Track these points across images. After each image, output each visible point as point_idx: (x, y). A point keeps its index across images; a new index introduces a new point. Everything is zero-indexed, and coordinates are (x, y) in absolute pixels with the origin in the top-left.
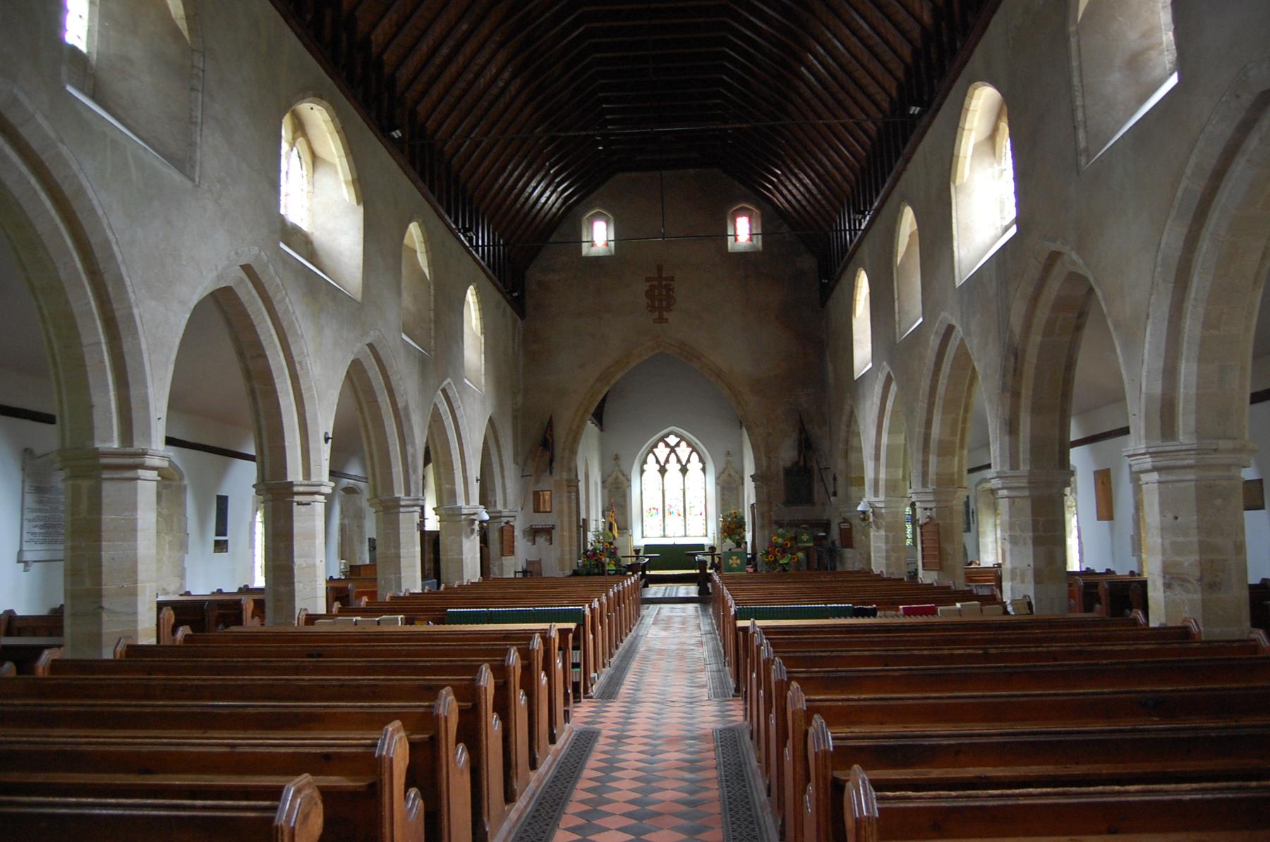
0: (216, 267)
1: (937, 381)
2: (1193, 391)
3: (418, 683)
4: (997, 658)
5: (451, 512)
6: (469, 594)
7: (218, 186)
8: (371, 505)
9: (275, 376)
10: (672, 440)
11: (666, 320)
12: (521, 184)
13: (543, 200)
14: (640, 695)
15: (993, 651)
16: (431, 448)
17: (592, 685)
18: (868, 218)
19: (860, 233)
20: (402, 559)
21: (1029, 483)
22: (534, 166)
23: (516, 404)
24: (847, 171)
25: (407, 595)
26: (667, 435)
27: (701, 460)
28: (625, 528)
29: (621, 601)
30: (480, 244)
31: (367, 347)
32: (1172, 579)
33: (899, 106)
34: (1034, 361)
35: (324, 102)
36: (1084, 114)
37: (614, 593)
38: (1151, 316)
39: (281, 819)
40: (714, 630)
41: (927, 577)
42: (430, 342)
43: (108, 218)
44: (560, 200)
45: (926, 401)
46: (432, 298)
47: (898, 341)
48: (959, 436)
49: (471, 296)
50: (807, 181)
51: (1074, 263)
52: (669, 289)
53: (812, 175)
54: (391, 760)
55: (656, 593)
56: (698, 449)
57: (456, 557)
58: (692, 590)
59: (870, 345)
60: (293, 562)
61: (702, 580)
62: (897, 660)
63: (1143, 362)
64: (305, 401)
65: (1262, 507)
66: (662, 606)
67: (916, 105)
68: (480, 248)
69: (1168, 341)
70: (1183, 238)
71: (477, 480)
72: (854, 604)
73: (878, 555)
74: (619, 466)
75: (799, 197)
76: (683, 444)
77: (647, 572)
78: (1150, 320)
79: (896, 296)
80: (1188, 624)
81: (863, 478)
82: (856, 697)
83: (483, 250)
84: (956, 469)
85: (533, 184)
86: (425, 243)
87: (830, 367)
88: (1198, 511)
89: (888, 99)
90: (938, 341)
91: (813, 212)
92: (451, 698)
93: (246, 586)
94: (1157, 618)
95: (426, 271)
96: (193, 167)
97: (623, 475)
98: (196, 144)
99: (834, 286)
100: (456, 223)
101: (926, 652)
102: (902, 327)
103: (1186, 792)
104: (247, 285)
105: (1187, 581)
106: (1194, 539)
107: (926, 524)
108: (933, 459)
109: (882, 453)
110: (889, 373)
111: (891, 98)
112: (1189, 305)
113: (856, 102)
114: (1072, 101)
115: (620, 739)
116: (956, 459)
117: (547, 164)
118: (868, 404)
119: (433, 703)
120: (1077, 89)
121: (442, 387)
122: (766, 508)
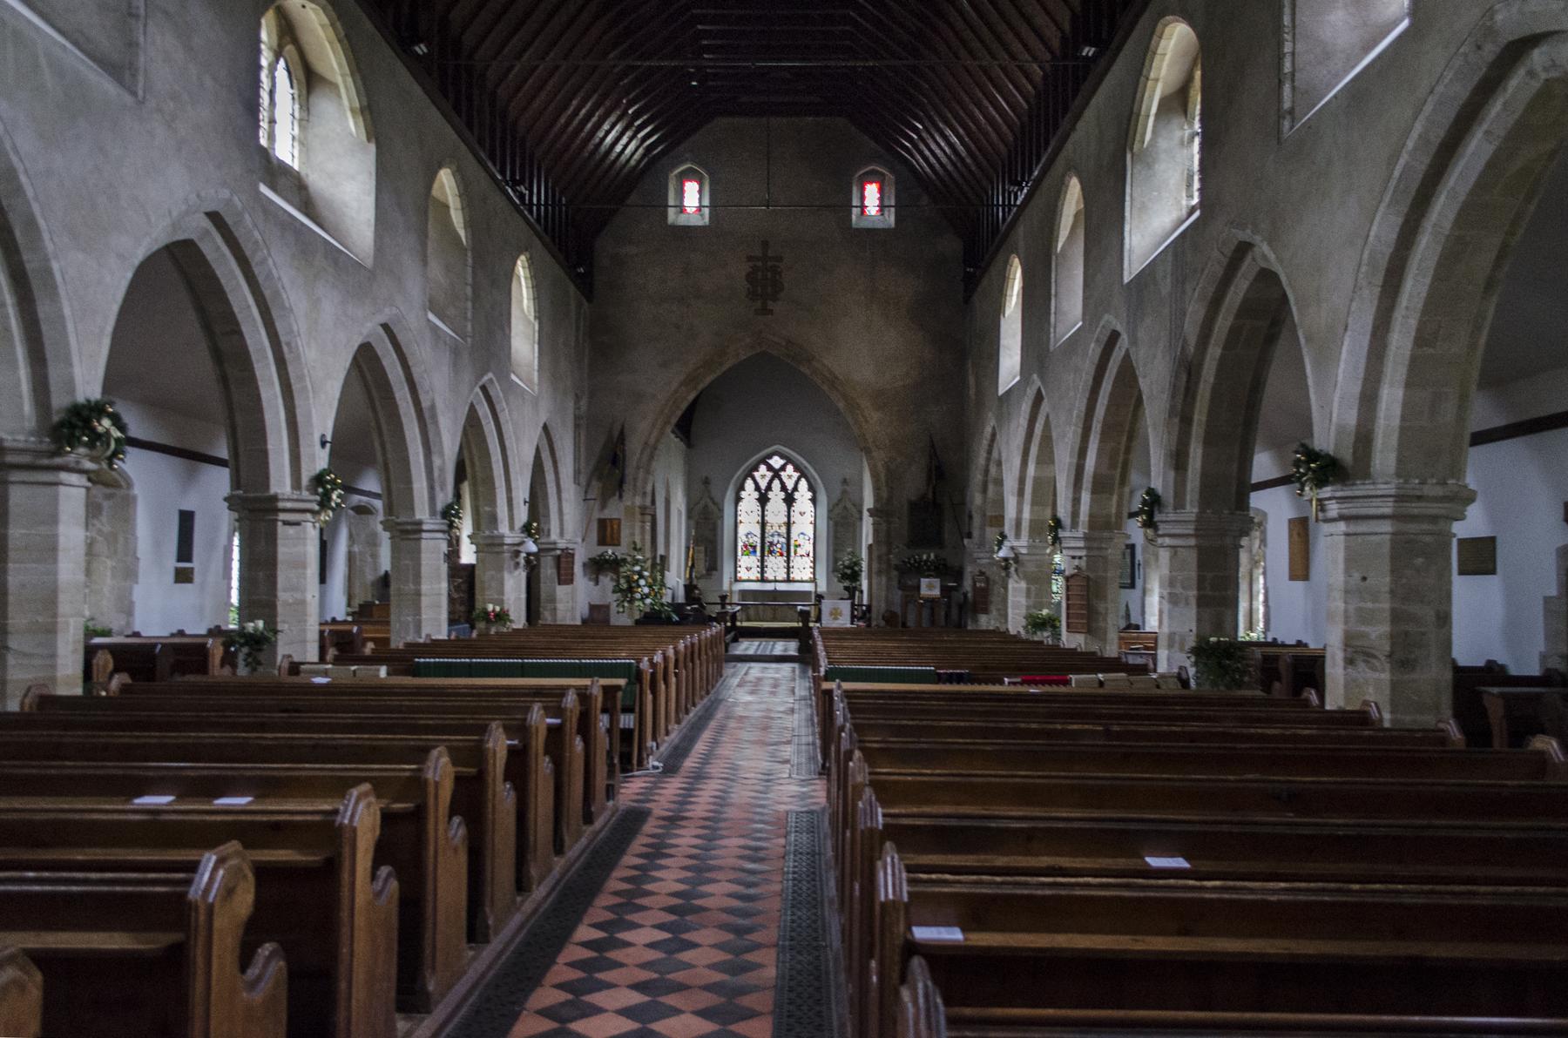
0: (170, 212)
1: (1096, 400)
2: (1396, 422)
3: (412, 743)
4: (1119, 736)
5: (489, 541)
6: (514, 644)
7: (172, 105)
8: (385, 530)
11: (771, 312)
12: (589, 125)
13: (618, 148)
15: (1116, 728)
16: (467, 463)
18: (1025, 191)
20: (423, 598)
21: (1196, 530)
22: (608, 103)
23: (579, 408)
24: (1005, 128)
25: (428, 641)
26: (770, 456)
27: (811, 488)
28: (713, 566)
29: (696, 655)
30: (535, 201)
32: (1356, 652)
33: (1072, 43)
34: (1212, 380)
37: (686, 647)
40: (811, 695)
41: (1071, 640)
42: (466, 326)
43: (11, 138)
44: (641, 151)
45: (1081, 425)
46: (469, 270)
47: (1052, 348)
48: (1119, 470)
49: (521, 269)
50: (954, 139)
51: (1265, 257)
53: (961, 131)
54: (354, 830)
55: (746, 649)
56: (809, 475)
57: (496, 597)
58: (791, 647)
60: (275, 596)
61: (802, 635)
62: (998, 733)
63: (1336, 385)
65: (1493, 572)
66: (753, 664)
68: (535, 208)
69: (1369, 358)
70: (1397, 229)
71: (525, 502)
74: (709, 492)
76: (790, 468)
77: (738, 624)
79: (1053, 292)
81: (1003, 517)
82: (928, 771)
83: (539, 210)
84: (1114, 511)
85: (606, 127)
86: (460, 196)
87: (972, 380)
88: (1392, 571)
90: (1099, 351)
92: (445, 760)
93: (218, 627)
94: (1335, 699)
95: (462, 233)
96: (134, 76)
97: (714, 503)
98: (137, 45)
100: (503, 173)
101: (1034, 726)
102: (1057, 330)
104: (213, 239)
105: (1375, 657)
106: (1386, 605)
107: (1073, 576)
108: (1086, 497)
109: (1026, 487)
111: (1063, 32)
112: (1398, 315)
113: (1018, 35)
114: (1280, 44)
115: (674, 820)
116: (1115, 498)
118: (1013, 425)
119: (421, 766)
120: (1286, 30)
121: (480, 383)
122: (884, 549)
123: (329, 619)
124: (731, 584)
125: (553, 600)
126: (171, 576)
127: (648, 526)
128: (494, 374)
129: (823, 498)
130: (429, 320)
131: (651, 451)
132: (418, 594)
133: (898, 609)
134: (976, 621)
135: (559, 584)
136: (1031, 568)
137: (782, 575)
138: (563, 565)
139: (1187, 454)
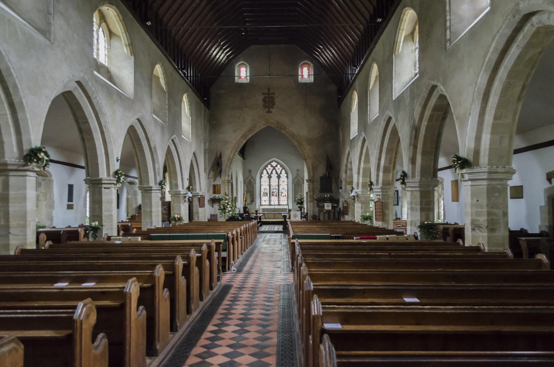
1: (384, 141)
2: (488, 146)
4: (394, 256)
9: (93, 132)
10: (274, 164)
11: (271, 112)
12: (207, 49)
13: (218, 56)
14: (253, 270)
15: (393, 254)
17: (231, 266)
18: (358, 69)
19: (355, 75)
21: (419, 185)
22: (214, 41)
23: (206, 147)
24: (351, 47)
25: (155, 228)
26: (272, 162)
27: (286, 173)
30: (189, 75)
31: (137, 120)
32: (475, 226)
33: (373, 18)
35: (114, 7)
36: (450, 23)
38: (471, 114)
39: (76, 316)
41: (377, 224)
44: (225, 57)
45: (379, 149)
46: (167, 99)
48: (392, 165)
49: (185, 98)
50: (334, 51)
51: (442, 91)
52: (273, 98)
53: (336, 48)
55: (265, 229)
57: (178, 212)
59: (357, 124)
60: (102, 213)
64: (107, 143)
66: (267, 234)
67: (380, 18)
68: (189, 78)
71: (188, 179)
72: (331, 234)
73: (358, 214)
74: (251, 175)
75: (330, 59)
76: (279, 166)
78: (471, 116)
80: (479, 246)
81: (353, 182)
83: (190, 78)
84: (391, 179)
85: (213, 49)
87: (341, 135)
88: (487, 198)
89: (369, 14)
90: (385, 124)
91: (336, 66)
92: (161, 269)
95: (164, 87)
96: (50, 34)
97: (253, 178)
99: (344, 99)
100: (178, 66)
101: (365, 254)
103: (449, 309)
105: (482, 228)
106: (485, 210)
107: (377, 202)
110: (364, 137)
112: (488, 109)
116: (391, 174)
117: (219, 40)
118: (356, 150)
121: (171, 139)
122: (312, 193)
123: (121, 221)
124: (259, 206)
125: (198, 213)
126: (66, 207)
127: (230, 187)
128: (176, 135)
129: (290, 176)
130: (153, 117)
131: (231, 161)
132: (151, 212)
133: (317, 214)
134: (344, 218)
135: (200, 207)
136: (362, 199)
137: (277, 203)
138: (201, 201)
139: (416, 159)
